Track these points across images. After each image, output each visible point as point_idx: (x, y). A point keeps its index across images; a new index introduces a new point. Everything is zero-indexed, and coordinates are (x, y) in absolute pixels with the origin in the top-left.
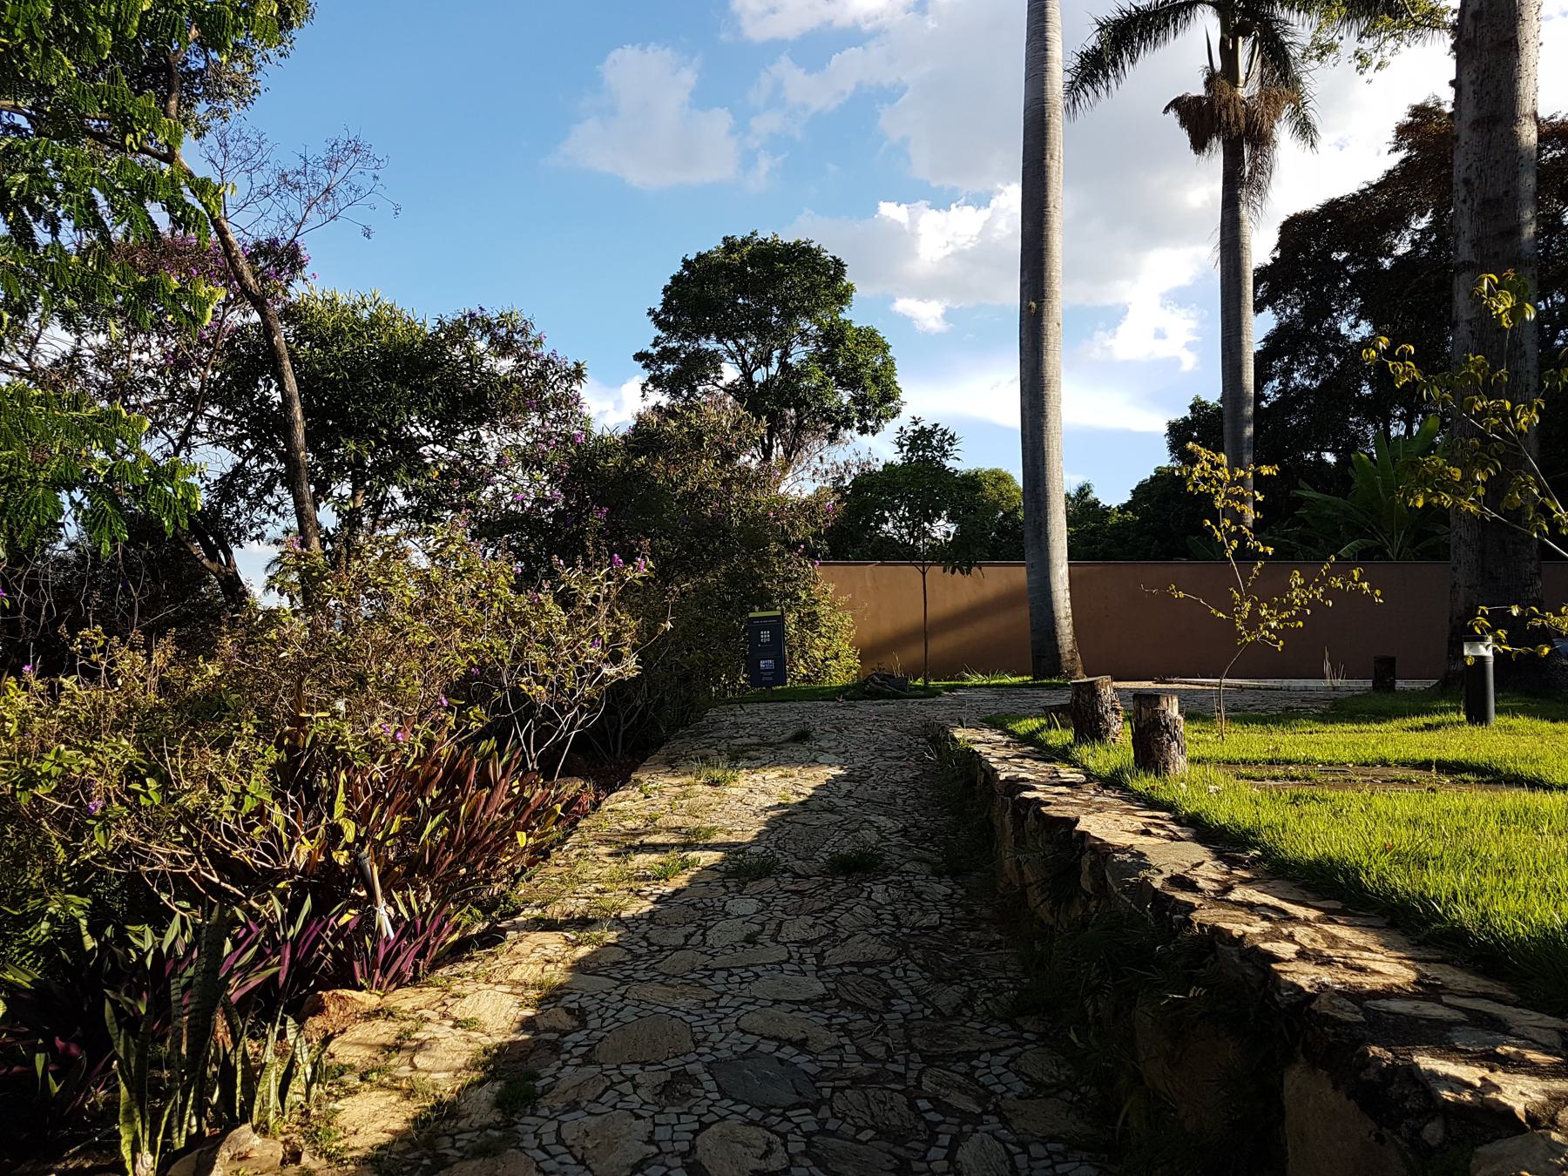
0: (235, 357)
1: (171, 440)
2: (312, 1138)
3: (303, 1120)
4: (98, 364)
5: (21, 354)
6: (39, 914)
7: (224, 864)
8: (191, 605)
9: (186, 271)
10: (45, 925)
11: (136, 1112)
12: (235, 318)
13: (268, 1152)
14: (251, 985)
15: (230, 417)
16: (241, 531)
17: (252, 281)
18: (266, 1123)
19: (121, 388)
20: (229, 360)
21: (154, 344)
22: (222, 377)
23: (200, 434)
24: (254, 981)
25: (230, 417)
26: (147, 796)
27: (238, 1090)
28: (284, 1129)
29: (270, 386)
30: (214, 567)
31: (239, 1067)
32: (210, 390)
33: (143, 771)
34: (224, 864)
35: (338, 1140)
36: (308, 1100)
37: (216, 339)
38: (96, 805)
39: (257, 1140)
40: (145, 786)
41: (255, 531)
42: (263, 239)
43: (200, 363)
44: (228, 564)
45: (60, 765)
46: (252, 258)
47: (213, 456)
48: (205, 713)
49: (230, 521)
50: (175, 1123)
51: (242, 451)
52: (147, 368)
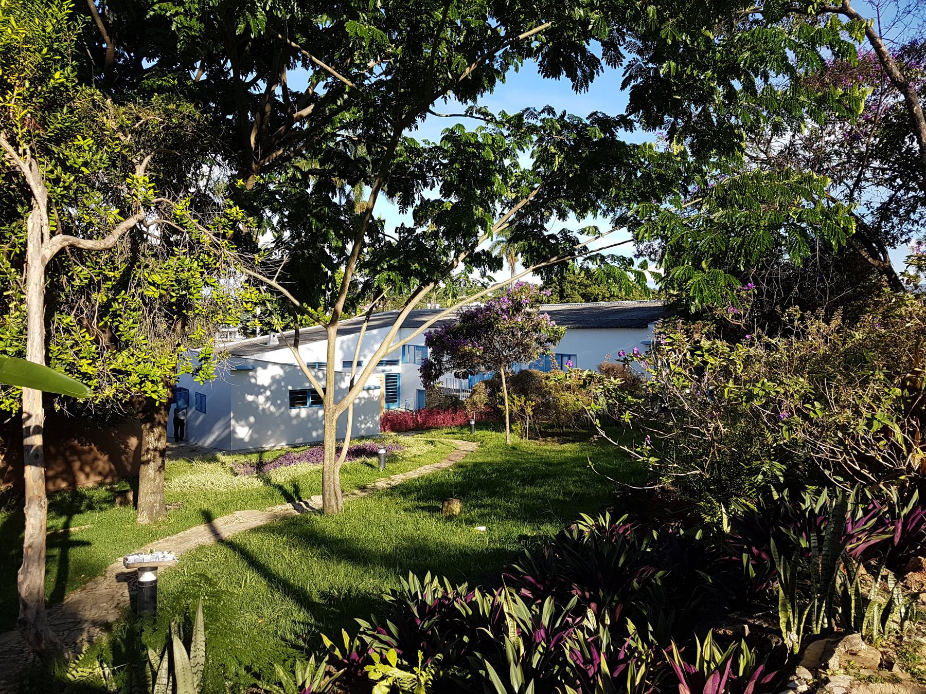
0: (890, 125)
1: (848, 187)
2: (902, 656)
3: (897, 642)
4: (805, 148)
5: (762, 151)
6: (757, 471)
7: (863, 459)
8: (863, 287)
9: (856, 78)
10: (760, 477)
11: (789, 606)
12: (889, 101)
13: (871, 656)
14: (872, 542)
15: (886, 166)
16: (895, 238)
17: (898, 74)
18: (871, 636)
19: (817, 162)
20: (885, 129)
21: (837, 129)
22: (880, 142)
23: (867, 180)
24: (874, 540)
25: (886, 166)
26: (815, 412)
27: (853, 611)
28: (884, 644)
29: (913, 140)
30: (876, 263)
31: (853, 597)
32: (872, 150)
33: (813, 397)
34: (863, 459)
35: (921, 664)
36: (902, 630)
37: (875, 118)
38: (784, 415)
39: (863, 646)
40: (813, 405)
41: (905, 237)
42: (906, 43)
43: (866, 134)
44: (885, 261)
45: (763, 390)
46: (899, 58)
47: (875, 193)
48: (854, 362)
49: (887, 233)
50: (814, 618)
51: (894, 187)
52: (833, 145)
